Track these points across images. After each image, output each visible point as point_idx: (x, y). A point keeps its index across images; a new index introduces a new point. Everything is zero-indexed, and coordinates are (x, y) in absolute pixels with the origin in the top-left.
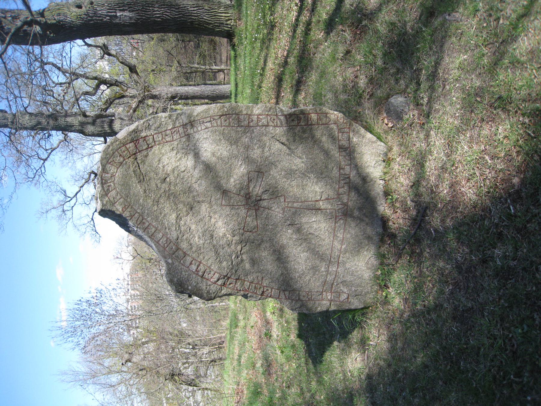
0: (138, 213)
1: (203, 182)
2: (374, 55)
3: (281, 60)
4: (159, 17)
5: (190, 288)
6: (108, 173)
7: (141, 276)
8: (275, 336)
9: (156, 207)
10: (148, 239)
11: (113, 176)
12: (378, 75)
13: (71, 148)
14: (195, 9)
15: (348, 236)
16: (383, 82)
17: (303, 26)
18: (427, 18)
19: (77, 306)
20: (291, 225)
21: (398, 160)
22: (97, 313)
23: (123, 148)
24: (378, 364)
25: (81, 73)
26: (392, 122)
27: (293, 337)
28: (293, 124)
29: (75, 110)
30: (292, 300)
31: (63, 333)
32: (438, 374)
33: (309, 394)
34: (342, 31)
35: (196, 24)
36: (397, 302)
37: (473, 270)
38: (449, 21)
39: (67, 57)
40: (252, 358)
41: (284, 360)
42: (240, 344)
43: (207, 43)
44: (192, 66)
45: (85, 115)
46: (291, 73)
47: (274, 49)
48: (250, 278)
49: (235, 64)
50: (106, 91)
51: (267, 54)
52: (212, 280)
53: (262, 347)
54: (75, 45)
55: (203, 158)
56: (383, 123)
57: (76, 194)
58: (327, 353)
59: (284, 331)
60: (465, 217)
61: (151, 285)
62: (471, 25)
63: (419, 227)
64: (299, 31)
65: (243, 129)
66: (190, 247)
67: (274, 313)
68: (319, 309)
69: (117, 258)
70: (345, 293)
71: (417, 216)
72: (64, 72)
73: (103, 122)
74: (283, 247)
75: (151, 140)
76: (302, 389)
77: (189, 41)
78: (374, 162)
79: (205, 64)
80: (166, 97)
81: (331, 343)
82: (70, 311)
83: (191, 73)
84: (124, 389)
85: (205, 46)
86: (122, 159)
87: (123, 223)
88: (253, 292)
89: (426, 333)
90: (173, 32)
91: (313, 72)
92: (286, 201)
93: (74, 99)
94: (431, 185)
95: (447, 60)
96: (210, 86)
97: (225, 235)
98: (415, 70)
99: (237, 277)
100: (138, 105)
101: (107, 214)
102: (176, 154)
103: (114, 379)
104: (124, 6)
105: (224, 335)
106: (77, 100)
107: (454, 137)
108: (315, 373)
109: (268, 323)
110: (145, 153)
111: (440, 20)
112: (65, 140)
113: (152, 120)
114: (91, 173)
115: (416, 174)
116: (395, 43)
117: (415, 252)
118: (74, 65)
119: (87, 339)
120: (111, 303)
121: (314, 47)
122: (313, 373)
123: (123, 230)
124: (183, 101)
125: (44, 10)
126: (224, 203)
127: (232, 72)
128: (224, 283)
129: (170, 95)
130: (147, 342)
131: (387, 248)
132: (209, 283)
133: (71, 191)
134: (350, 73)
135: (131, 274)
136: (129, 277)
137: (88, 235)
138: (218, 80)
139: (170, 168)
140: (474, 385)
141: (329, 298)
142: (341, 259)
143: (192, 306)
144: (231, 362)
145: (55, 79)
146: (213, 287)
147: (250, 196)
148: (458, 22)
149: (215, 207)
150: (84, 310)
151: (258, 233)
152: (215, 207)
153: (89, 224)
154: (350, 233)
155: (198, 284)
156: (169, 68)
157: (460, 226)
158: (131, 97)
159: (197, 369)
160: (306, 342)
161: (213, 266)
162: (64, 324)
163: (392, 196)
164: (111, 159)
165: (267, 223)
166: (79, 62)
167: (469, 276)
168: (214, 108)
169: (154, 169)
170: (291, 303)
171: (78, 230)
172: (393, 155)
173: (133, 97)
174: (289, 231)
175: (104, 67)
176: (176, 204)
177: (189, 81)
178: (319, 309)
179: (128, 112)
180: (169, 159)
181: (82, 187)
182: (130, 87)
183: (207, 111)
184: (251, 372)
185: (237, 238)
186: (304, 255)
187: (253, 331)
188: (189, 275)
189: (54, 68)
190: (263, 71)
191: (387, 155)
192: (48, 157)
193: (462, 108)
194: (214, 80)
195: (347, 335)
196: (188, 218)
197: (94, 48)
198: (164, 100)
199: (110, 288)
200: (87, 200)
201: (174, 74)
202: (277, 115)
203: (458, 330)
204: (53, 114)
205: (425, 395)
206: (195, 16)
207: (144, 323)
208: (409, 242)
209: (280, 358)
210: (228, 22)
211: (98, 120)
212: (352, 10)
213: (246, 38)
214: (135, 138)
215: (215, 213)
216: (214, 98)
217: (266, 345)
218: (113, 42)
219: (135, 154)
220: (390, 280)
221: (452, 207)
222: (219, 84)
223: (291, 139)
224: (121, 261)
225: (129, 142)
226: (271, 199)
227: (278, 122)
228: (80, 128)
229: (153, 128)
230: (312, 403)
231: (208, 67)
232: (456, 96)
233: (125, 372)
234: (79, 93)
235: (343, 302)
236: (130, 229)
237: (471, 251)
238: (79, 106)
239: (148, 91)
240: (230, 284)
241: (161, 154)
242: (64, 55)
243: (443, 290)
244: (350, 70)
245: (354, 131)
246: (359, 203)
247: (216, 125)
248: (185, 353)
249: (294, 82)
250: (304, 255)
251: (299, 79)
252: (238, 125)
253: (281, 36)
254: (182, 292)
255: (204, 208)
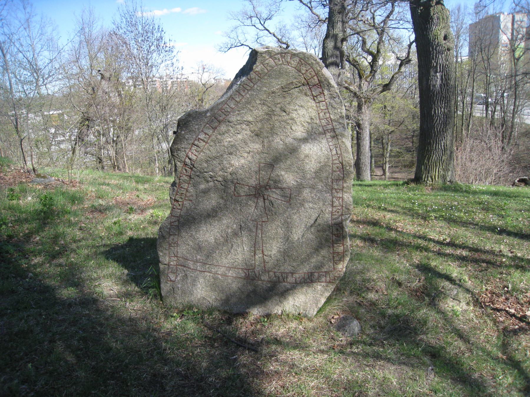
0: (254, 86)
1: (282, 146)
2: (397, 307)
3: (393, 225)
5: (183, 132)
6: (291, 58)
7: (186, 92)
8: (130, 217)
9: (259, 102)
10: (229, 94)
11: (288, 63)
12: (378, 310)
13: (312, 26)
14: (443, 147)
15: (230, 281)
16: (372, 315)
17: (424, 245)
18: (430, 352)
19: (156, 27)
20: (241, 228)
21: (301, 327)
22: (150, 47)
23: (313, 74)
24: (108, 310)
25: (384, 37)
26: (335, 322)
27: (130, 233)
28: (334, 230)
29: (348, 31)
30: (170, 229)
31: (130, 14)
32: (102, 361)
33: (75, 247)
34: (420, 279)
35: (428, 148)
36: (167, 326)
37: (201, 391)
38: (427, 370)
39: (399, 25)
40: (108, 196)
41: (106, 224)
42: (120, 185)
43: (411, 159)
44: (389, 144)
45: (344, 40)
46: (381, 234)
47: (404, 219)
48: (191, 189)
49: (391, 185)
50: (366, 61)
51: (399, 213)
52: (190, 153)
53: (120, 205)
54: (411, 33)
55: (303, 146)
56: (335, 313)
57: (267, 30)
58: (116, 264)
59: (136, 225)
60: (249, 384)
61: (176, 100)
62: (423, 388)
63: (238, 346)
64: (420, 241)
65: (330, 184)
66: (221, 132)
67: (152, 216)
68: (161, 254)
69: (204, 69)
70: (176, 278)
71: (249, 344)
72: (384, 22)
73: (337, 57)
74: (220, 220)
75: (320, 99)
76: (79, 241)
77: (413, 142)
78: (298, 305)
79: (390, 156)
80: (360, 118)
81: (126, 268)
82: (152, 20)
83: (383, 144)
84: (74, 72)
85: (408, 157)
86: (304, 72)
87: (245, 71)
88: (177, 192)
89: (140, 351)
90: (421, 127)
91: (381, 254)
92: (263, 223)
93: (359, 30)
94: (277, 356)
95: (393, 368)
96: (369, 161)
97: (232, 165)
98: (383, 343)
99: (192, 177)
100: (352, 92)
101: (253, 57)
102: (307, 122)
103: (85, 62)
104: (446, 80)
105: (127, 171)
106: (358, 33)
107: (322, 374)
108: (96, 253)
109: (142, 211)
110: (309, 93)
111: (428, 362)
112: (319, 21)
113: (339, 101)
114: (287, 45)
115: (288, 342)
116: (408, 325)
117: (215, 342)
118: (391, 31)
119: (125, 36)
120: (160, 61)
121: (405, 255)
122: (96, 251)
123: (237, 72)
124: (355, 135)
125: (442, 5)
126: (262, 165)
127: (382, 182)
128: (186, 165)
129: (361, 122)
130: (120, 95)
131: (218, 317)
132: (187, 151)
133: (271, 25)
134: (381, 285)
135: (187, 81)
136: (185, 80)
137: (226, 40)
138: (375, 170)
139: (294, 116)
140: (93, 392)
141: (172, 263)
142: (208, 274)
143: (155, 140)
144: (102, 177)
145: (378, 13)
146: (183, 154)
147: (267, 189)
148: (426, 376)
149: (258, 157)
150: (153, 34)
151: (234, 197)
152: (258, 157)
153: (237, 41)
154: (232, 282)
155: (187, 140)
156: (388, 122)
157: (240, 381)
158: (360, 85)
159: (92, 144)
160: (126, 245)
161: (204, 154)
162: (139, 14)
163: (266, 322)
164: (303, 62)
165: (242, 205)
166: (395, 36)
167: (194, 388)
168: (350, 158)
169: (294, 101)
170: (166, 227)
171: (232, 31)
172: (305, 322)
173: (360, 87)
174: (235, 225)
175: (389, 61)
176: (261, 121)
177: (374, 141)
178: (161, 254)
179: (346, 82)
180: (304, 112)
181: (274, 35)
182: (369, 84)
183: (347, 151)
184: (93, 194)
185: (229, 177)
186: (212, 240)
187: (134, 197)
188: (195, 132)
189: (388, 12)
190: (383, 209)
191: (305, 317)
192: (304, 4)
193: (349, 381)
194: (375, 166)
195: (135, 282)
196: (248, 132)
197: (407, 50)
198: (357, 117)
199: (174, 61)
200: (261, 40)
201: (382, 127)
202: (342, 215)
203: (144, 379)
204: (345, 9)
205: (81, 350)
206: (436, 147)
207: (139, 93)
208: (224, 336)
209: (109, 222)
210: (429, 178)
211: (338, 53)
212: (438, 288)
213: (415, 195)
214: (322, 84)
215: (253, 157)
216: (358, 165)
217: (120, 209)
218: (412, 69)
219: (308, 84)
220: (188, 319)
221: (258, 373)
222: (372, 171)
223: (320, 228)
224: (201, 71)
225: (319, 78)
226: (265, 208)
227: (335, 216)
228: (331, 35)
229: (332, 101)
230: (66, 251)
231: (388, 160)
232: (359, 375)
233: (91, 73)
234: (364, 35)
235: (168, 276)
236: (238, 78)
237: (217, 389)
238: (352, 35)
239: (365, 102)
240: (186, 170)
241: (308, 108)
242: (401, 22)
243: (180, 366)
244: (383, 286)
245: (327, 286)
246: (263, 288)
247: (334, 159)
248: (109, 132)
249: (372, 237)
250: (212, 240)
251: (375, 241)
252: (335, 177)
253: (416, 226)
254: (179, 125)
255: (256, 146)
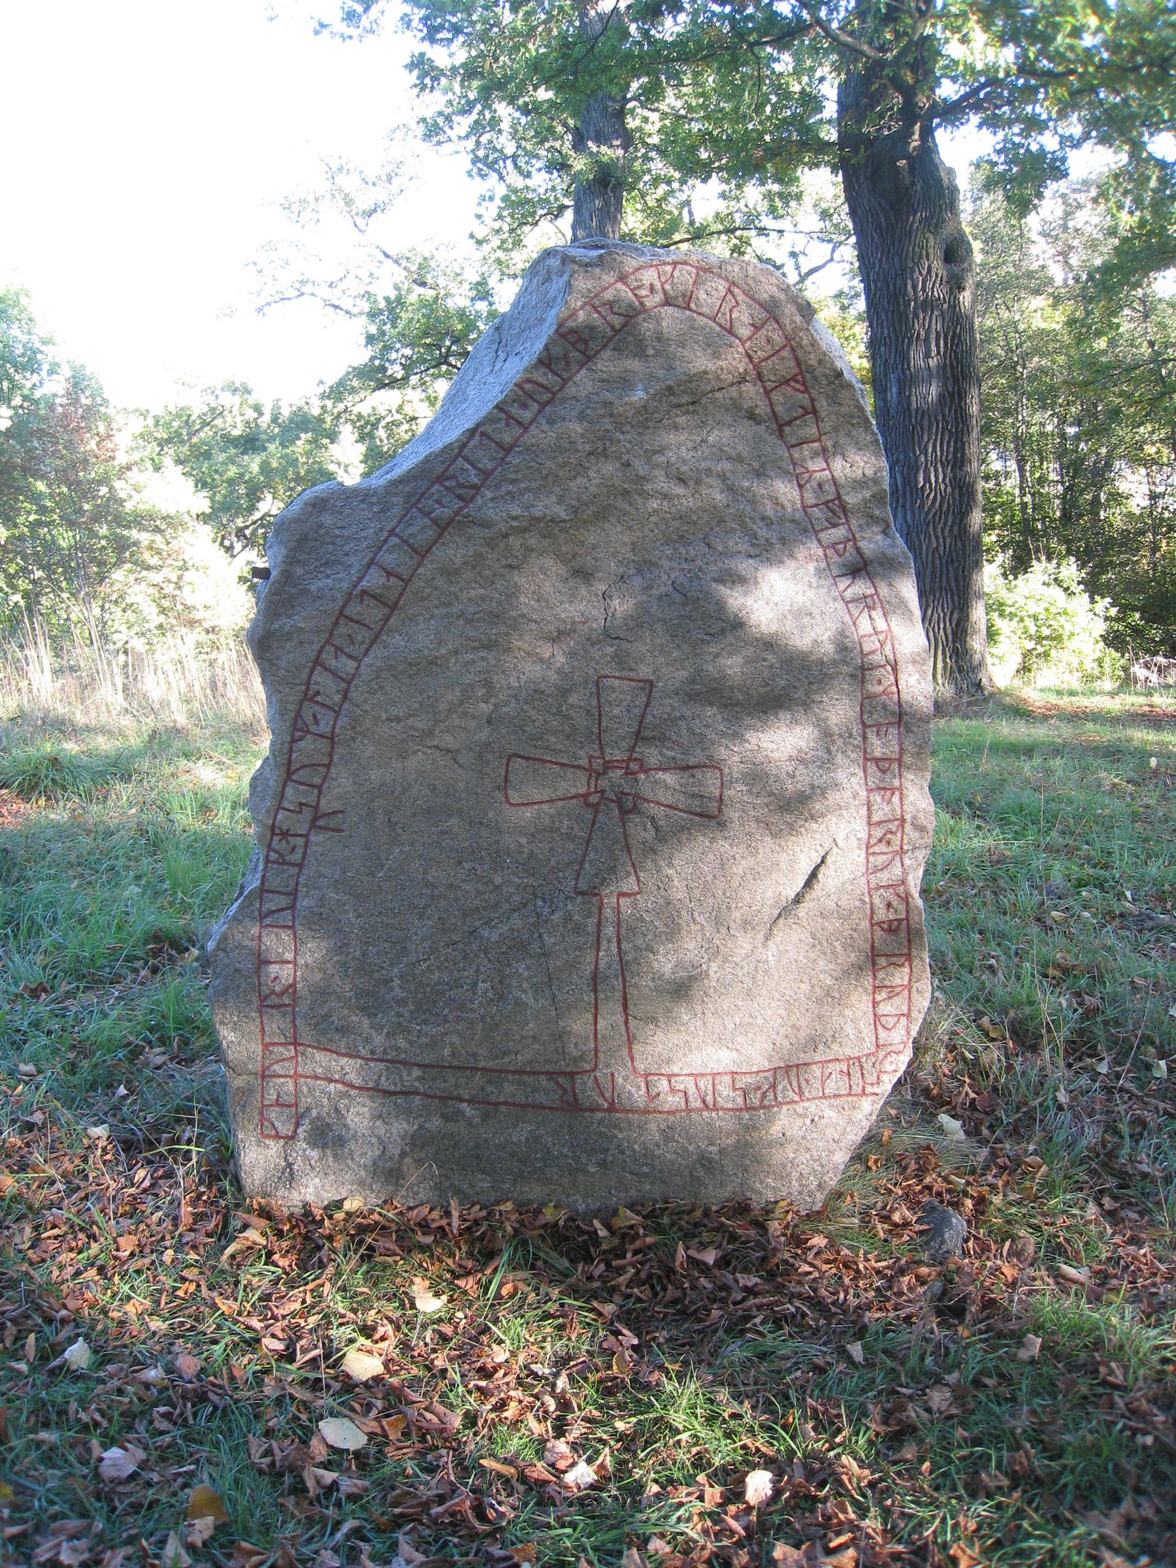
4: (927, 479)
219: (760, 376)
